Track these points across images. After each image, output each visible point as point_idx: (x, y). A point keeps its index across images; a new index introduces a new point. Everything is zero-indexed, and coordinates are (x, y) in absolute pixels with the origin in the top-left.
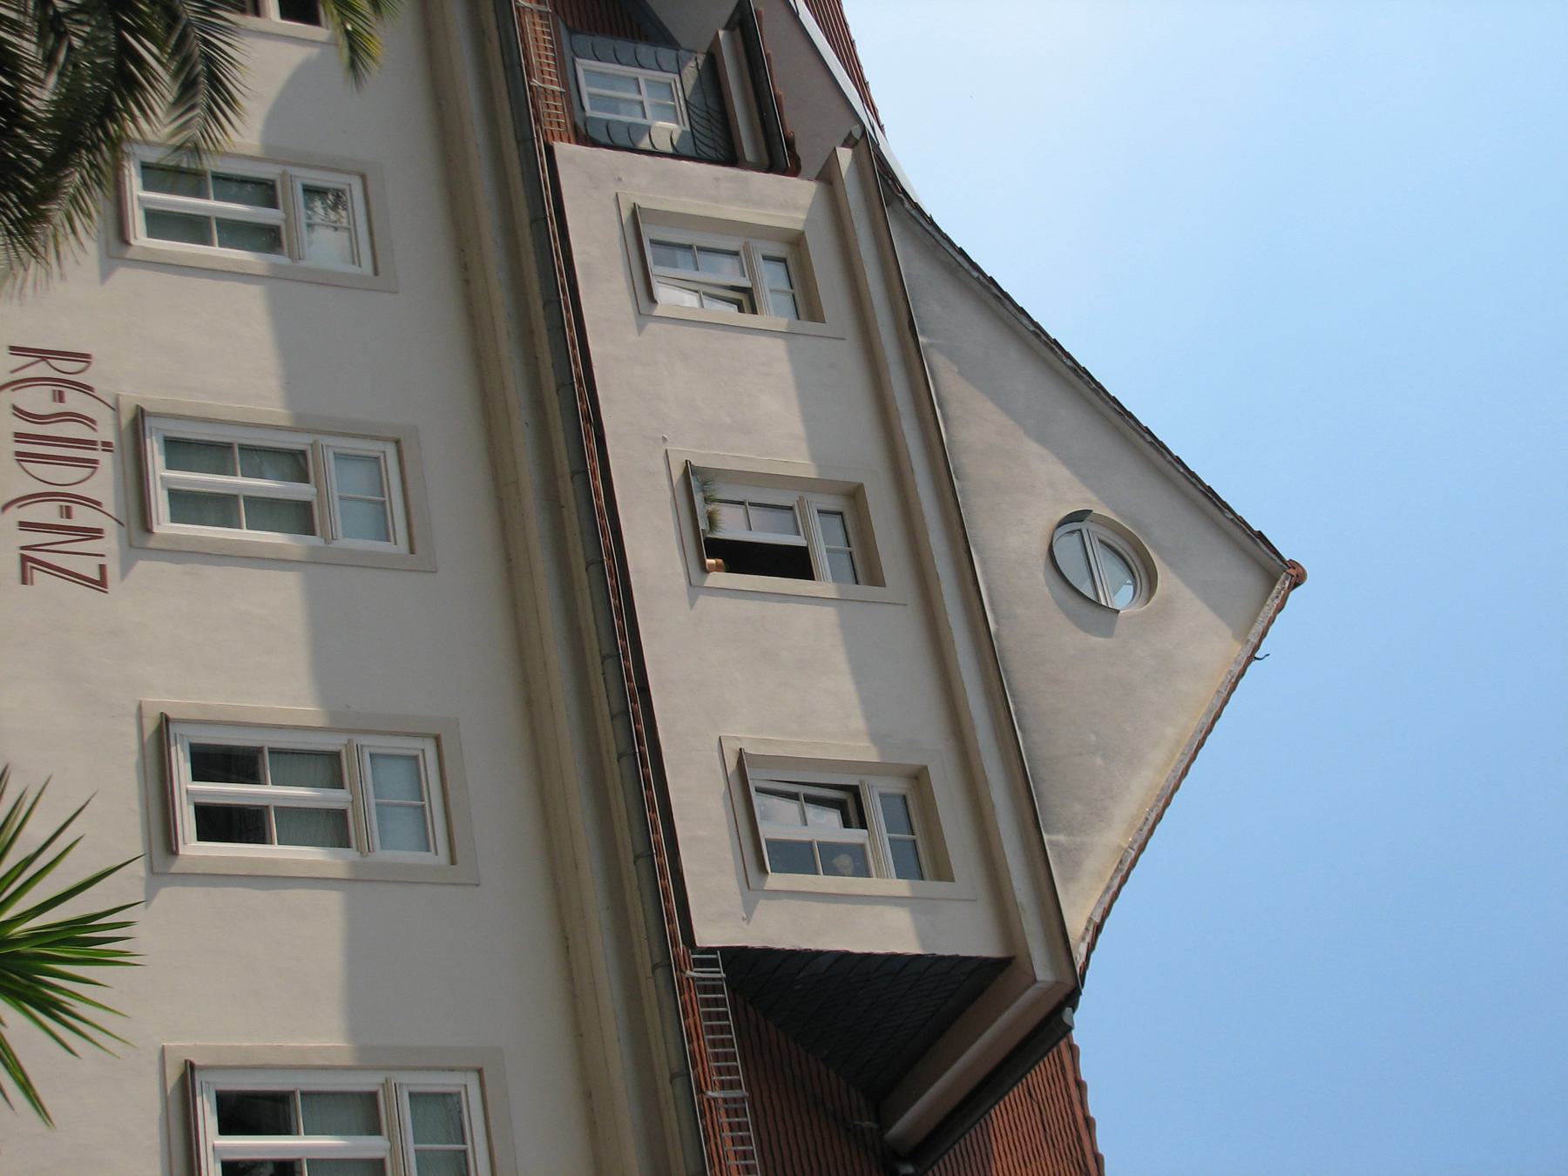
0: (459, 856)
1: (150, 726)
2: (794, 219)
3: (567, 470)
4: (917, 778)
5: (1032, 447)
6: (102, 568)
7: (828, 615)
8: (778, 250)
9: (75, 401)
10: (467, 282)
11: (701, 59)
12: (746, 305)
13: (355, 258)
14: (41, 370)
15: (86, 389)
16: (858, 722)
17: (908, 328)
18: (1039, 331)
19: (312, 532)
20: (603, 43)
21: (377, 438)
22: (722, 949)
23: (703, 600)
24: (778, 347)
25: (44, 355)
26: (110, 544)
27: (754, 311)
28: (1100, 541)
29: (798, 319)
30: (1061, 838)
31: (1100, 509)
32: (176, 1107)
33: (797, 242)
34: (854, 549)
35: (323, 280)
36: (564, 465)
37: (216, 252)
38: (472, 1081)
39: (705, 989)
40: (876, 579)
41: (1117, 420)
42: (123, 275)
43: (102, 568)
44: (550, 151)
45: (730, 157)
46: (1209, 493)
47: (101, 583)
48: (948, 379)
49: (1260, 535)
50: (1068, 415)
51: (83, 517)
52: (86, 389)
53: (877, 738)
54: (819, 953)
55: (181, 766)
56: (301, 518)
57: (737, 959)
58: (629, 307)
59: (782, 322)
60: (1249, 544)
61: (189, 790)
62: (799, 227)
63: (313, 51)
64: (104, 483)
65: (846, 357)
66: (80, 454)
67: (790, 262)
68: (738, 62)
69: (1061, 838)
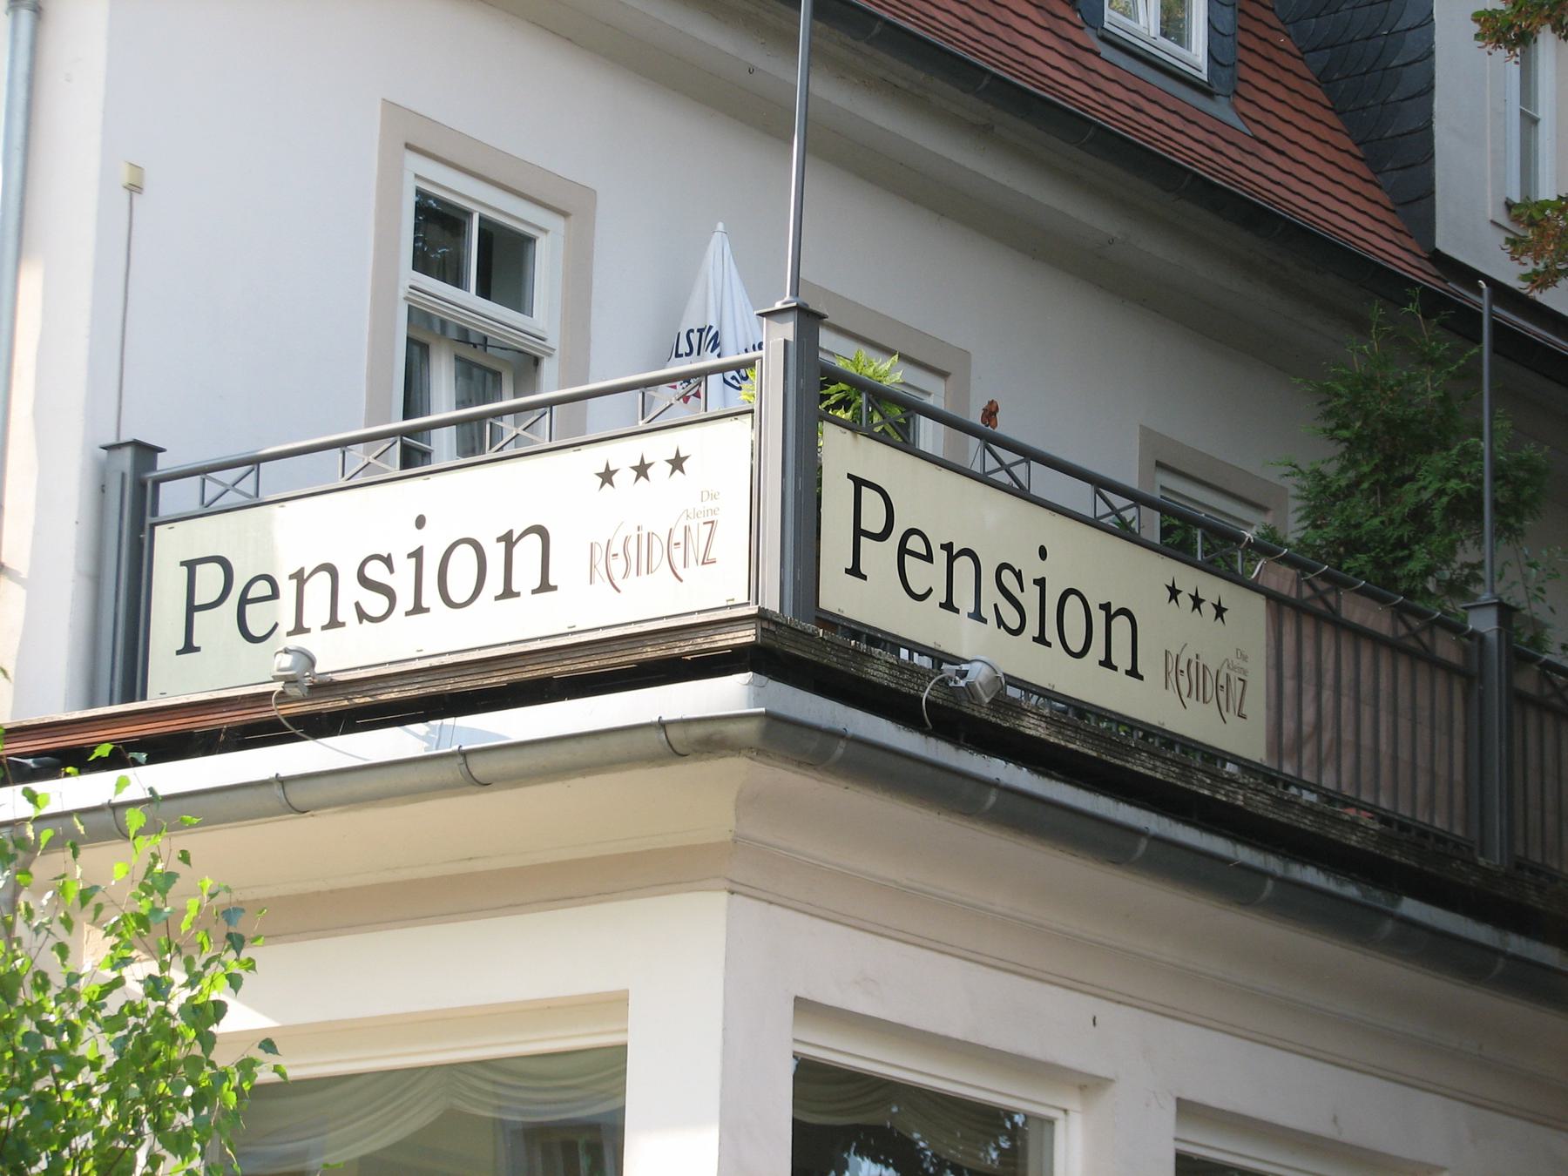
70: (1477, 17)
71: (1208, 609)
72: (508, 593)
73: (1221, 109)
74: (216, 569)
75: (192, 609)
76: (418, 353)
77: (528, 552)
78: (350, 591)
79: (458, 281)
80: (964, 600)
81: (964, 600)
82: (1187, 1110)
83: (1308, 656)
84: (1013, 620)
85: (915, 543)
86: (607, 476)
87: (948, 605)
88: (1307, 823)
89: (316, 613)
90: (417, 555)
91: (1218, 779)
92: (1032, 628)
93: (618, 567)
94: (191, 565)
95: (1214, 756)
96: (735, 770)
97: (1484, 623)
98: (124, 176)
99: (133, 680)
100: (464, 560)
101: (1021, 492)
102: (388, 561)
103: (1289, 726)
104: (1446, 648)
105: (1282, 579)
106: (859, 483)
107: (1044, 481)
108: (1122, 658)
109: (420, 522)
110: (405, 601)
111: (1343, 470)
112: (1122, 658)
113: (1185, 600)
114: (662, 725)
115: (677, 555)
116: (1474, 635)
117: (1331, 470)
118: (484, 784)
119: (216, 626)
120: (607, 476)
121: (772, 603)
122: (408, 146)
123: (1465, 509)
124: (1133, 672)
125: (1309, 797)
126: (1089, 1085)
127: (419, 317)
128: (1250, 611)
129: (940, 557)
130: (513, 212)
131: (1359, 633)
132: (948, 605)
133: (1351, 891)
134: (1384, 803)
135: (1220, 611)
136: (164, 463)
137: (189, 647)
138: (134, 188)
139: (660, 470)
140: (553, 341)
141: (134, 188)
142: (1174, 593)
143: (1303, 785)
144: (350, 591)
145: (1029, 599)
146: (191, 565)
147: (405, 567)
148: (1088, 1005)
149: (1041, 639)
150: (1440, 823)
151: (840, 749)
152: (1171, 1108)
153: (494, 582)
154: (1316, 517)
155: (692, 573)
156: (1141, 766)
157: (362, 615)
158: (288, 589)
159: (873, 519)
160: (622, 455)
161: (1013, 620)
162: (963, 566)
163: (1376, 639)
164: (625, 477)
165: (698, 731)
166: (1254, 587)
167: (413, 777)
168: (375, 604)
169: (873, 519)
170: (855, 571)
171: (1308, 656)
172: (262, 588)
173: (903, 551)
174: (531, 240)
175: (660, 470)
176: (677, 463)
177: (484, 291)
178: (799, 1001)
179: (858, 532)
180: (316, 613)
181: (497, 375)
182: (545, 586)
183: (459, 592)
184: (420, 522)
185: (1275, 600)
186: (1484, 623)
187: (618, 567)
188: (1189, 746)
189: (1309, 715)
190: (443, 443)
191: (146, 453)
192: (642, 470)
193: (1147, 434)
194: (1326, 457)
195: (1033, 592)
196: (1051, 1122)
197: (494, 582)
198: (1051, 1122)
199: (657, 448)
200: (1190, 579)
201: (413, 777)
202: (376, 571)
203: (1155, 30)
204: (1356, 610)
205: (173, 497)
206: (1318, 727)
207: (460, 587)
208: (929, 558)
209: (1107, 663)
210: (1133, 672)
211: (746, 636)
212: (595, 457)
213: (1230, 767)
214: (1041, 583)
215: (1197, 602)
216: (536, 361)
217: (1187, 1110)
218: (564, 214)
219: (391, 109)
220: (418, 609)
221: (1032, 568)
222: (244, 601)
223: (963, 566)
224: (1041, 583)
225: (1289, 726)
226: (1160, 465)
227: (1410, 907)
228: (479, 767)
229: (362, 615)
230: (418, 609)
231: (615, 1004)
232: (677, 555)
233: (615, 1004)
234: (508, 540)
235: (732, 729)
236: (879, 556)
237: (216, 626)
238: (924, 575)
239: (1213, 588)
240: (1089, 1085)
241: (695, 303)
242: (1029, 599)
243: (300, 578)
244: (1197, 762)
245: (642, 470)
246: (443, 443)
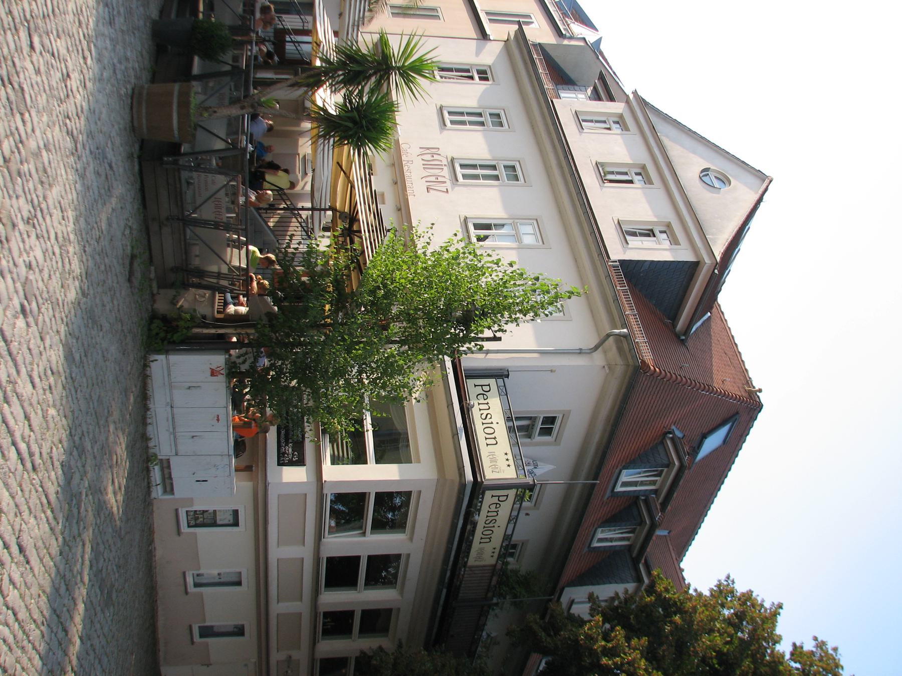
0: (526, 180)
1: (462, 219)
2: (620, 111)
3: (589, 233)
4: (668, 226)
5: (692, 155)
6: (447, 189)
7: (639, 191)
8: (616, 119)
9: (436, 157)
10: (533, 129)
11: (592, 88)
12: (651, 235)
13: (537, 241)
14: (428, 151)
15: (439, 155)
16: (650, 213)
17: (653, 129)
18: (690, 130)
19: (499, 180)
20: (564, 86)
21: (514, 161)
22: (619, 261)
23: (604, 189)
24: (619, 137)
25: (428, 149)
26: (448, 184)
27: (660, 244)
28: (715, 177)
29: (645, 184)
30: (710, 236)
31: (712, 167)
32: (439, 112)
33: (621, 116)
34: (670, 239)
35: (529, 247)
36: (588, 232)
37: (468, 127)
38: (518, 163)
39: (614, 267)
40: (651, 183)
41: (715, 148)
42: (445, 132)
43: (447, 189)
44: (552, 101)
45: (599, 99)
46: (743, 162)
47: (447, 191)
48: (666, 142)
49: (759, 171)
50: (701, 148)
51: (440, 179)
52: (439, 155)
53: (656, 216)
54: (645, 261)
55: (471, 228)
56: (496, 178)
57: (623, 263)
58: (577, 131)
59: (619, 131)
60: (756, 173)
61: (473, 232)
62: (621, 112)
63: (489, 86)
64: (446, 172)
65: (638, 138)
66: (440, 167)
67: (667, 232)
68: (602, 87)
69: (710, 236)
70: (593, 592)
71: (492, 554)
72: (486, 439)
73: (586, 549)
74: (489, 389)
75: (482, 386)
76: (530, 418)
77: (493, 441)
78: (485, 412)
79: (542, 424)
80: (490, 514)
81: (490, 514)
82: (408, 555)
83: (486, 571)
84: (487, 522)
85: (498, 506)
86: (506, 454)
87: (488, 512)
88: (457, 573)
89: (482, 407)
90: (492, 423)
91: (463, 558)
92: (486, 526)
93: (491, 457)
94: (489, 385)
95: (468, 557)
96: (457, 479)
97: (495, 600)
98: (554, 369)
99: (468, 377)
100: (491, 431)
101: (509, 523)
102: (491, 418)
103: (473, 569)
104: (490, 595)
105: (499, 566)
106: (507, 496)
107: (511, 526)
108: (483, 541)
109: (497, 423)
110: (484, 421)
111: (520, 575)
112: (483, 541)
113: (493, 551)
114: (464, 467)
115: (494, 467)
116: (492, 599)
117: (521, 573)
118: (453, 437)
119: (479, 390)
120: (506, 454)
121: (484, 483)
122: (564, 415)
123: (515, 596)
124: (480, 543)
125: (462, 573)
126: (411, 539)
127: (535, 418)
128: (492, 561)
129: (496, 510)
130: (555, 432)
131: (491, 580)
132: (488, 512)
133: (446, 581)
134: (463, 585)
135: (492, 556)
136: (506, 379)
137: (475, 386)
138: (551, 371)
139: (507, 463)
140: (534, 440)
141: (551, 371)
142: (494, 549)
143: (465, 571)
144: (485, 412)
145: (491, 525)
146: (489, 385)
147: (490, 421)
148: (424, 538)
149: (484, 527)
150: (460, 595)
151: (462, 496)
152: (408, 553)
153: (488, 436)
154: (512, 571)
155: (490, 470)
156: (464, 545)
157: (482, 414)
158: (486, 402)
159: (501, 499)
160: (510, 457)
161: (487, 522)
162: (496, 514)
163: (490, 583)
164: (506, 457)
165: (463, 473)
166: (497, 561)
167: (454, 426)
168: (483, 417)
169: (501, 499)
170: (492, 496)
171: (486, 571)
172: (485, 397)
173: (497, 504)
174: (550, 435)
175: (507, 463)
176: (509, 466)
177: (541, 428)
178: (420, 491)
179: (499, 496)
180: (482, 407)
181: (527, 431)
182: (487, 445)
183: (486, 430)
184: (497, 423)
185: (495, 566)
186: (495, 600)
187: (491, 457)
188: (469, 553)
189: (476, 572)
190: (511, 424)
191: (507, 376)
192: (507, 460)
193: (528, 541)
194: (523, 572)
195: (492, 525)
196: (405, 533)
197: (488, 436)
198: (405, 533)
199: (511, 462)
200: (497, 551)
201: (454, 426)
202: (489, 416)
203: (599, 537)
204: (495, 579)
205: (500, 381)
206: (475, 574)
207: (487, 431)
208: (496, 508)
209: (481, 538)
210: (480, 543)
211: (479, 480)
212: (509, 452)
213: (466, 559)
214: (494, 527)
215: (493, 552)
216: (530, 438)
217: (408, 555)
218: (555, 441)
219: (569, 411)
220: (483, 424)
221: (496, 525)
222: (483, 394)
223: (496, 514)
224: (494, 527)
225: (473, 569)
226: (523, 544)
227: (445, 591)
228: (456, 436)
229: (482, 414)
230: (483, 424)
231: (419, 461)
232: (494, 467)
233: (419, 461)
234: (495, 438)
235: (463, 478)
236: (495, 500)
237: (479, 390)
238: (493, 508)
239: (496, 555)
240: (411, 539)
241: (542, 464)
242: (491, 525)
243: (488, 403)
244: (466, 554)
245: (507, 460)
246: (511, 424)
